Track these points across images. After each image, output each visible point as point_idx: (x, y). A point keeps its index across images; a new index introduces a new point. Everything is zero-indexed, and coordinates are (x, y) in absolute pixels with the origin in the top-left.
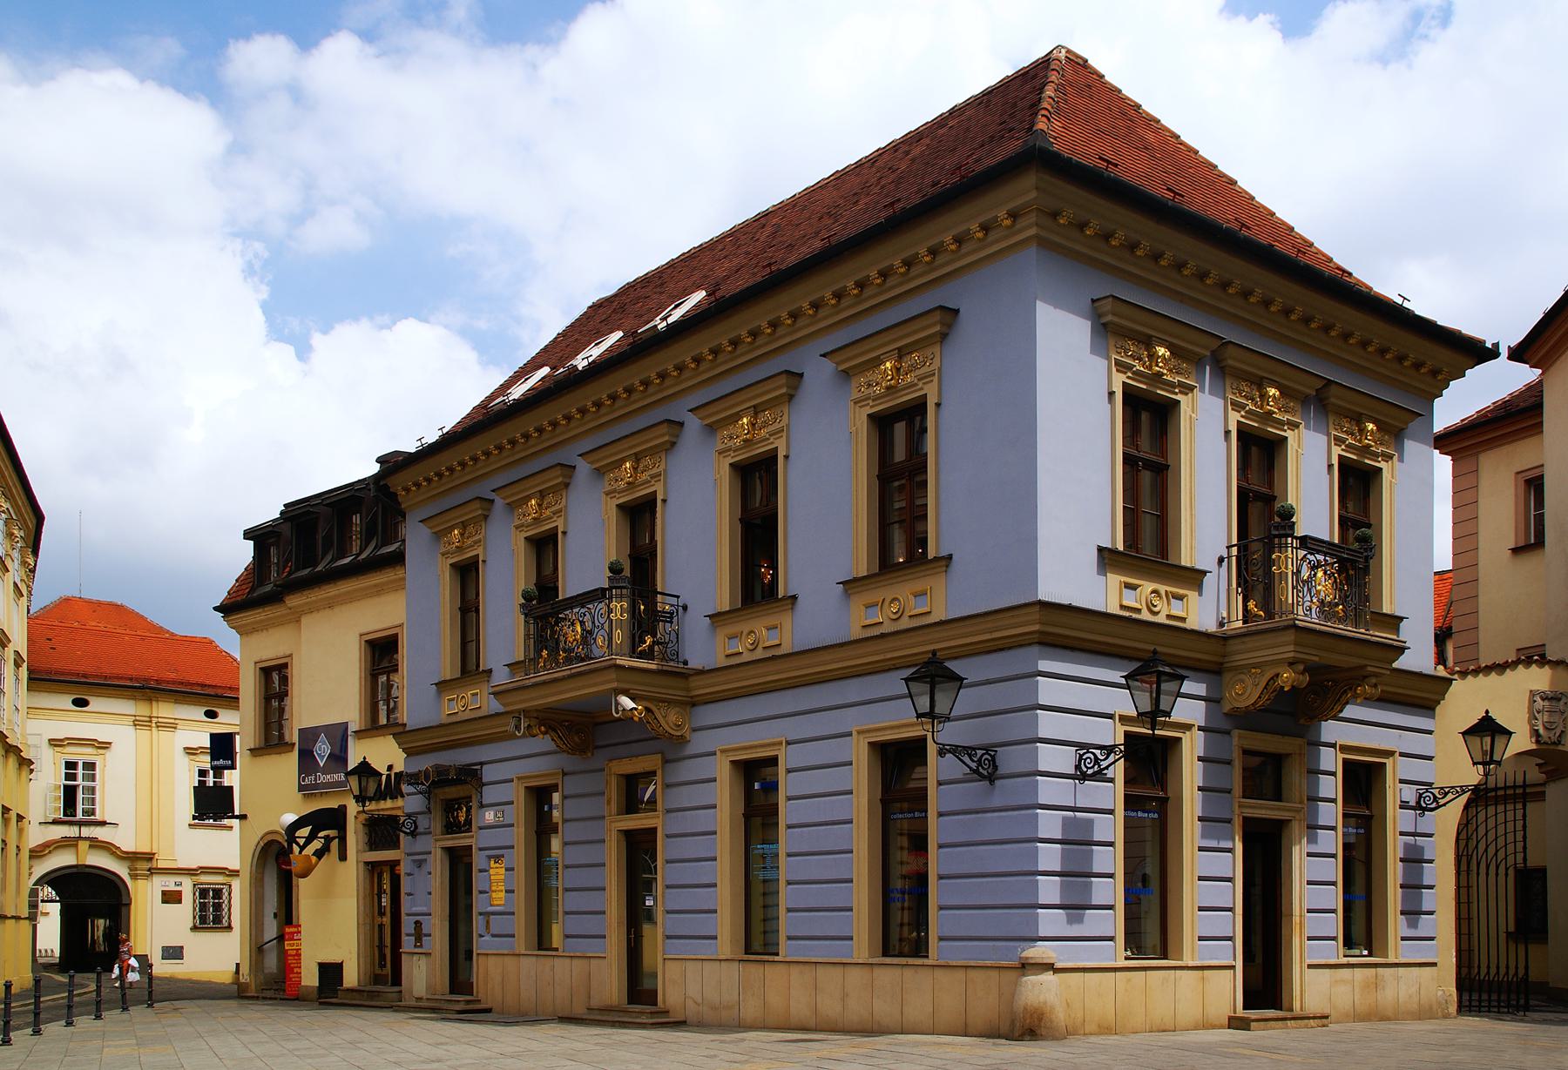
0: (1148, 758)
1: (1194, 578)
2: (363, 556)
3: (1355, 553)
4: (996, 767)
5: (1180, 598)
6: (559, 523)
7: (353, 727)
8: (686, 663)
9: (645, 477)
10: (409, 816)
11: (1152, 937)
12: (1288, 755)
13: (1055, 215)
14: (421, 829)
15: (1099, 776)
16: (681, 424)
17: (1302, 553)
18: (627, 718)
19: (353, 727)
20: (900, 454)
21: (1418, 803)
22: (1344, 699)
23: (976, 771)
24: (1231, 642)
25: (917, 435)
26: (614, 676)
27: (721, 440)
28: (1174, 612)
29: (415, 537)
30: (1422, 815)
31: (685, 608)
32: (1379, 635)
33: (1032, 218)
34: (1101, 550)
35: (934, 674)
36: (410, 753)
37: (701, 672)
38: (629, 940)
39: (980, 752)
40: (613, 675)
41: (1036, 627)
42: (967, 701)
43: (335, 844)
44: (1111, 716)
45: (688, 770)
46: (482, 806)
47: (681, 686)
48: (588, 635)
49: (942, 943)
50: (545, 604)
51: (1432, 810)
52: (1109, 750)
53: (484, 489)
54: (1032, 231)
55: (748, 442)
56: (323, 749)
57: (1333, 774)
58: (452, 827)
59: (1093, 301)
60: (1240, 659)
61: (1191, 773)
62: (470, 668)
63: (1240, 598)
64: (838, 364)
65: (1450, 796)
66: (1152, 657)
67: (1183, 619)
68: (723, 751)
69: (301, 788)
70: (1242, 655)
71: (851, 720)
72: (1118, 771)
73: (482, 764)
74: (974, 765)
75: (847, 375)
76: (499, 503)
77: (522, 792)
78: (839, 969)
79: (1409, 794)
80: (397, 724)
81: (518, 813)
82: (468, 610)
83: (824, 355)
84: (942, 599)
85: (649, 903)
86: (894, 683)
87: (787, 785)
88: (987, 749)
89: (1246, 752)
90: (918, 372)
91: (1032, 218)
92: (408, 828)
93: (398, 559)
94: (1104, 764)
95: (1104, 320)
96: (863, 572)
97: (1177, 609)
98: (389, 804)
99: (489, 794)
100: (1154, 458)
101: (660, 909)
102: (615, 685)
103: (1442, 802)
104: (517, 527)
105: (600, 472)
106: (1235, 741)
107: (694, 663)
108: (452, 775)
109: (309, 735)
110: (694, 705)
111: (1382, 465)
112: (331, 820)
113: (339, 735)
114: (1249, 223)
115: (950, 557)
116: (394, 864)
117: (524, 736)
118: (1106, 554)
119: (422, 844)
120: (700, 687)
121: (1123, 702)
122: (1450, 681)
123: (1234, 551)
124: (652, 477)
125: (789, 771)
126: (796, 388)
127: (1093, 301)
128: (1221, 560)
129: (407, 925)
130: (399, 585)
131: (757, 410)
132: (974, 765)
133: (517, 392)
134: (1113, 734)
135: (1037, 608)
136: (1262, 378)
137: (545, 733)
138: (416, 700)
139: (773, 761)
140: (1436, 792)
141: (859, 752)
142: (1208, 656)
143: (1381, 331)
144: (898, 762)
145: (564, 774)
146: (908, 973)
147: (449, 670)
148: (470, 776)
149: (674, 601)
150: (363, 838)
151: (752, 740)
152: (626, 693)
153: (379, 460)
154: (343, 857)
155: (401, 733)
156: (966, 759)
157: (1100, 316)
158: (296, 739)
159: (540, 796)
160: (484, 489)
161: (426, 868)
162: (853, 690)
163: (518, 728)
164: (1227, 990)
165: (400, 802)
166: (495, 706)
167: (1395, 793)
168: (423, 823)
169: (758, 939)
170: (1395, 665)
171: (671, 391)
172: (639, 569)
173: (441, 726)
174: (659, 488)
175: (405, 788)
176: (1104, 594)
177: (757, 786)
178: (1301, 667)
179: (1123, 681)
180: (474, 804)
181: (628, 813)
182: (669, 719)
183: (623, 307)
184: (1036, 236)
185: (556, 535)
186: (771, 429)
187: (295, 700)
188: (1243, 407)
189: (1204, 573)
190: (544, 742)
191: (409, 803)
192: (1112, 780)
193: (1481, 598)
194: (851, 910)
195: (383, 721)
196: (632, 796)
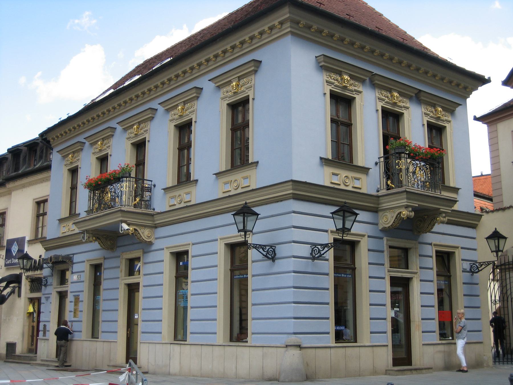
0: (345, 249)
1: (365, 170)
3: (434, 161)
4: (275, 254)
5: (358, 179)
6: (109, 151)
7: (27, 239)
8: (154, 209)
9: (142, 131)
11: (180, 337)
12: (410, 248)
13: (298, 23)
14: (49, 283)
15: (320, 257)
17: (409, 160)
18: (126, 235)
19: (27, 239)
20: (240, 120)
21: (471, 269)
22: (432, 223)
23: (266, 256)
24: (381, 198)
25: (246, 111)
26: (120, 215)
27: (222, 93)
28: (355, 186)
29: (55, 158)
30: (472, 275)
31: (155, 186)
32: (446, 194)
33: (288, 24)
34: (321, 158)
35: (246, 212)
36: (47, 249)
37: (159, 213)
38: (127, 334)
39: (267, 248)
40: (119, 214)
41: (291, 192)
42: (260, 225)
43: (17, 289)
44: (326, 231)
45: (151, 257)
46: (72, 273)
47: (155, 221)
48: (113, 200)
51: (477, 272)
52: (326, 245)
53: (81, 139)
54: (289, 30)
55: (181, 116)
56: (15, 249)
57: (431, 257)
59: (316, 57)
60: (385, 205)
61: (363, 257)
63: (384, 179)
65: (483, 266)
66: (346, 207)
67: (360, 189)
68: (167, 248)
69: (6, 265)
70: (386, 204)
72: (330, 254)
73: (73, 254)
75: (219, 87)
76: (87, 144)
78: (200, 346)
79: (467, 266)
81: (87, 276)
83: (209, 80)
84: (256, 179)
85: (136, 317)
87: (192, 263)
88: (271, 247)
89: (391, 247)
90: (246, 86)
91: (288, 24)
92: (44, 282)
93: (48, 168)
94: (322, 252)
95: (321, 64)
97: (357, 184)
98: (38, 272)
99: (76, 268)
100: (346, 121)
101: (140, 320)
102: (121, 219)
103: (480, 269)
104: (93, 153)
105: (125, 130)
106: (385, 242)
107: (158, 210)
108: (60, 259)
109: (11, 242)
110: (156, 227)
111: (446, 125)
112: (16, 279)
113: (20, 241)
114: (352, 14)
115: (257, 162)
116: (39, 299)
117: (86, 242)
118: (323, 161)
120: (159, 220)
121: (330, 225)
122: (481, 216)
123: (382, 159)
124: (145, 131)
125: (253, 262)
126: (200, 94)
127: (316, 57)
128: (376, 164)
129: (41, 328)
130: (47, 179)
132: (265, 253)
134: (328, 239)
135: (291, 183)
136: (391, 89)
137: (95, 240)
139: (186, 252)
140: (477, 264)
141: (220, 248)
142: (373, 204)
143: (440, 72)
144: (237, 251)
145: (105, 259)
146: (239, 349)
149: (150, 183)
150: (28, 288)
151: (178, 243)
152: (125, 222)
154: (19, 296)
155: (43, 241)
156: (261, 250)
157: (319, 63)
158: (5, 244)
159: (97, 268)
160: (81, 139)
163: (83, 238)
164: (385, 356)
167: (459, 266)
168: (50, 280)
169: (180, 333)
170: (453, 208)
174: (146, 135)
175: (45, 266)
176: (324, 177)
177: (181, 263)
178: (410, 209)
179: (331, 215)
181: (129, 276)
182: (145, 234)
183: (146, 66)
185: (192, 122)
186: (190, 110)
187: (7, 227)
188: (333, 84)
189: (369, 169)
190: (96, 245)
191: (46, 272)
192: (327, 260)
193: (502, 182)
194: (216, 320)
195: (40, 236)
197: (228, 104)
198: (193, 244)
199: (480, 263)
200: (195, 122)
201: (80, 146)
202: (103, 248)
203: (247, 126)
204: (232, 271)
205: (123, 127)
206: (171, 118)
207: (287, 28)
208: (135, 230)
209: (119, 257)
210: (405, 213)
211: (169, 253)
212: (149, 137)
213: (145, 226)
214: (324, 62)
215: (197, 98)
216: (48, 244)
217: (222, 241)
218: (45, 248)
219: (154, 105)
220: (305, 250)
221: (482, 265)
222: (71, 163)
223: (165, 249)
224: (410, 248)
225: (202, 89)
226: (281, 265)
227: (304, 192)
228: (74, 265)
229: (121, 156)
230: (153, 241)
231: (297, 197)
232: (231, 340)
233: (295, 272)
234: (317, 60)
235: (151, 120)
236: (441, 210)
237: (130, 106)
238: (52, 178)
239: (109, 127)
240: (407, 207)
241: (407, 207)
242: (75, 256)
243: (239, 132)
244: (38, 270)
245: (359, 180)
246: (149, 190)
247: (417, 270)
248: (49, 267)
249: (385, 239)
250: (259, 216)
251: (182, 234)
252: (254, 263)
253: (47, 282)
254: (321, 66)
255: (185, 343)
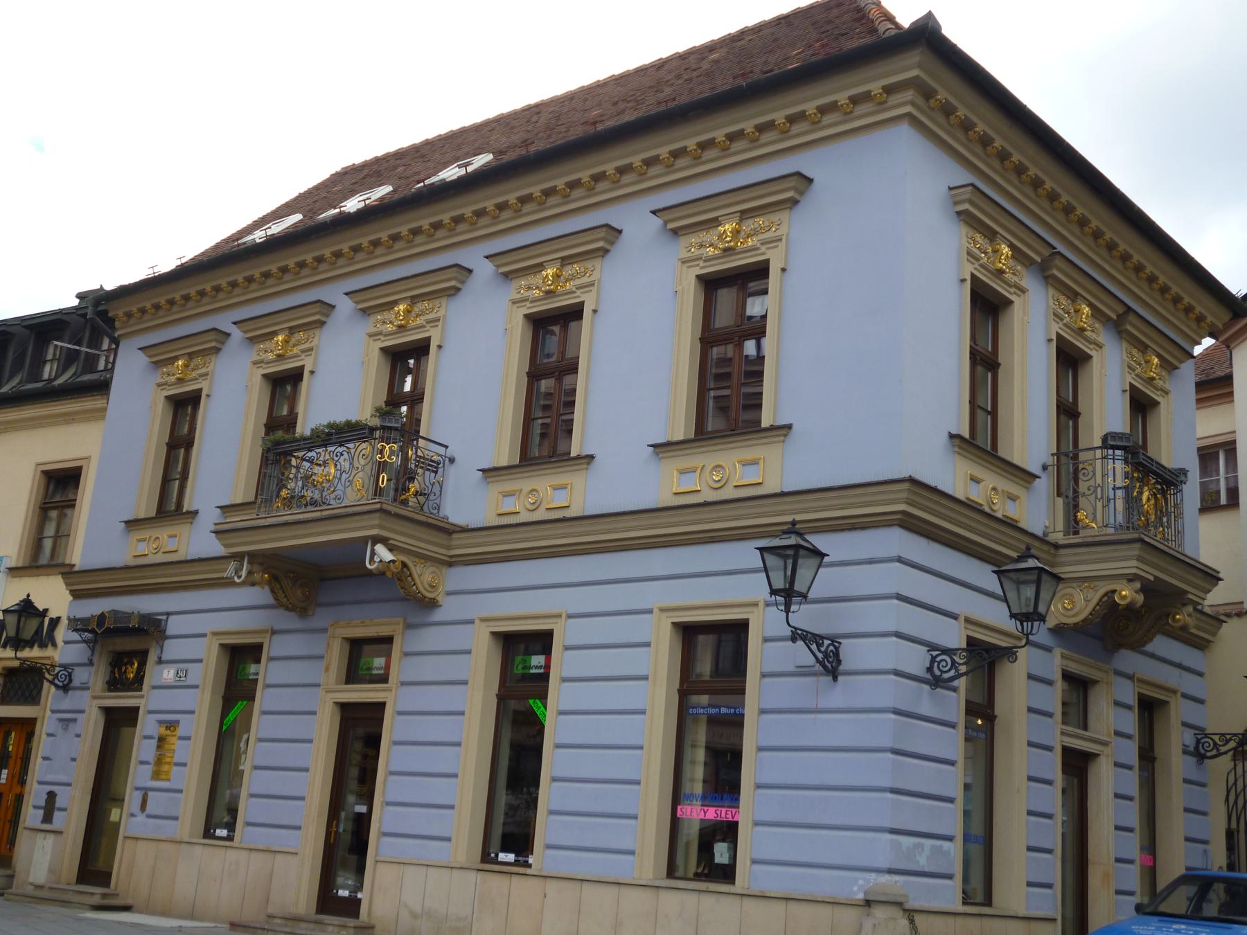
1: (1026, 477)
2: (56, 383)
6: (203, 385)
10: (65, 667)
14: (76, 683)
16: (228, 335)
21: (1197, 748)
24: (1063, 551)
26: (376, 522)
27: (370, 325)
31: (452, 460)
34: (952, 436)
36: (77, 595)
42: (826, 581)
45: (430, 638)
46: (160, 661)
49: (756, 867)
50: (281, 442)
58: (115, 684)
59: (950, 189)
62: (170, 507)
64: (498, 266)
71: (653, 595)
73: (168, 614)
74: (820, 656)
77: (215, 649)
78: (578, 884)
79: (1189, 738)
80: (63, 565)
81: (207, 673)
82: (179, 446)
83: (234, 323)
86: (747, 554)
87: (562, 663)
88: (834, 640)
90: (761, 237)
91: (909, 95)
93: (102, 387)
96: (680, 436)
99: (172, 649)
102: (375, 532)
103: (1223, 749)
108: (134, 623)
110: (450, 565)
115: (789, 427)
117: (243, 584)
119: (70, 701)
120: (462, 547)
131: (414, 300)
132: (820, 656)
133: (258, 236)
138: (94, 536)
140: (1216, 738)
145: (274, 632)
147: (145, 507)
148: (151, 629)
149: (441, 450)
151: (522, 609)
152: (384, 541)
153: (81, 296)
155: (68, 572)
156: (814, 647)
161: (75, 728)
162: (658, 561)
165: (49, 652)
166: (215, 548)
168: (80, 676)
171: (134, 329)
172: (400, 415)
173: (127, 568)
180: (152, 658)
181: (347, 682)
182: (423, 576)
184: (909, 115)
185: (200, 397)
188: (977, 259)
190: (259, 594)
196: (361, 657)
197: (527, 316)
198: (570, 616)
199: (1223, 735)
200: (440, 347)
201: (216, 340)
202: (279, 605)
203: (573, 368)
204: (684, 694)
205: (360, 306)
206: (373, 330)
207: (904, 103)
208: (404, 565)
209: (325, 630)
210: (1127, 594)
211: (669, 626)
212: (442, 338)
213: (425, 558)
214: (971, 202)
215: (217, 350)
216: (83, 583)
217: (665, 614)
218: (71, 591)
219: (224, 322)
220: (916, 660)
221: (1227, 741)
222: (728, 251)
223: (477, 622)
224: (1095, 682)
225: (620, 232)
226: (840, 693)
227: (921, 512)
228: (167, 642)
229: (342, 383)
230: (439, 599)
231: (909, 523)
232: (671, 873)
233: (897, 712)
234: (953, 196)
235: (449, 296)
236: (1190, 596)
237: (244, 294)
238: (110, 413)
239: (319, 301)
240: (1131, 579)
241: (1131, 579)
242: (172, 618)
243: (404, 409)
244: (32, 647)
245: (1014, 500)
246: (434, 466)
247: (1109, 735)
248: (85, 641)
249: (1058, 652)
250: (826, 559)
251: (871, 562)
252: (766, 680)
253: (71, 681)
254: (959, 213)
255: (528, 871)
